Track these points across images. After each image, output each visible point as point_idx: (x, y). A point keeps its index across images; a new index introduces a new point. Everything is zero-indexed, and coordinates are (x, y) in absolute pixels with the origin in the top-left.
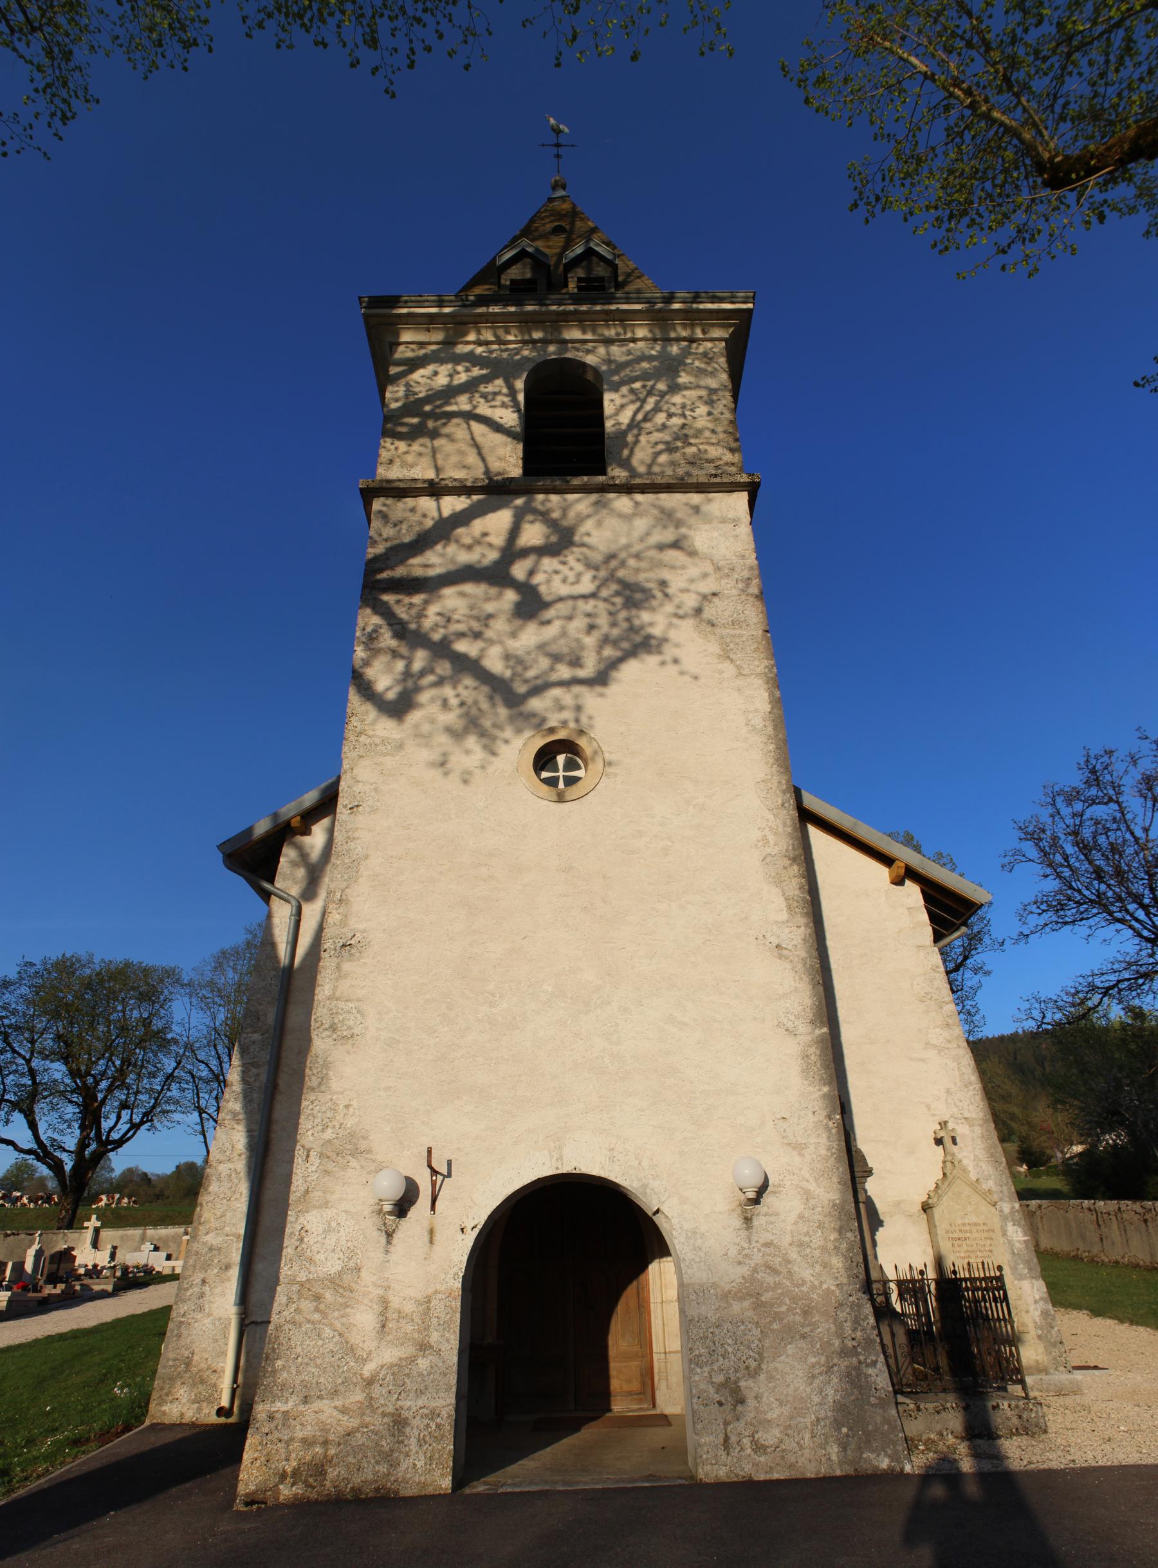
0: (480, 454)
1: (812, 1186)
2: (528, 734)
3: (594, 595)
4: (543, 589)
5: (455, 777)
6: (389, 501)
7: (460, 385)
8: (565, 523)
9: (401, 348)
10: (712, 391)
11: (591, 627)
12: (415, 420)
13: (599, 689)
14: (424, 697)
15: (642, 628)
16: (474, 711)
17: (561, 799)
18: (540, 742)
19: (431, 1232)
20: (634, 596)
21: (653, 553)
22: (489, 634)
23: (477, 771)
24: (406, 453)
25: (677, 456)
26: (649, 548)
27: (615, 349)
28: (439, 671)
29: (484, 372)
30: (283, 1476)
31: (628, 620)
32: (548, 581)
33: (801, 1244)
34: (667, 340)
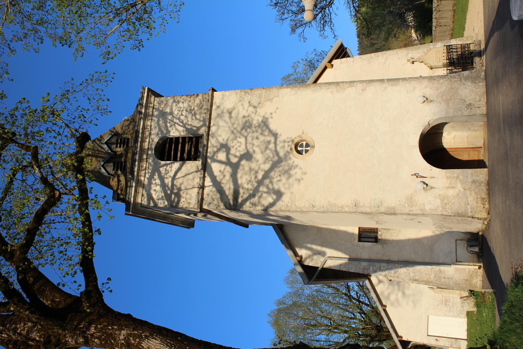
0: (189, 174)
1: (424, 86)
2: (291, 156)
3: (246, 138)
4: (242, 153)
5: (303, 177)
6: (204, 203)
7: (161, 182)
8: (219, 147)
9: (143, 202)
10: (174, 101)
11: (257, 138)
12: (173, 196)
13: (278, 135)
14: (276, 187)
15: (259, 124)
16: (283, 172)
17: (313, 147)
18: (295, 152)
19: (431, 177)
20: (247, 125)
21: (232, 120)
22: (256, 168)
23: (303, 170)
24: (186, 198)
25: (197, 112)
26: (231, 121)
27: (153, 132)
28: (268, 183)
29: (157, 174)
30: (484, 207)
31: (256, 127)
32: (239, 151)
33: (437, 89)
34: (152, 115)
